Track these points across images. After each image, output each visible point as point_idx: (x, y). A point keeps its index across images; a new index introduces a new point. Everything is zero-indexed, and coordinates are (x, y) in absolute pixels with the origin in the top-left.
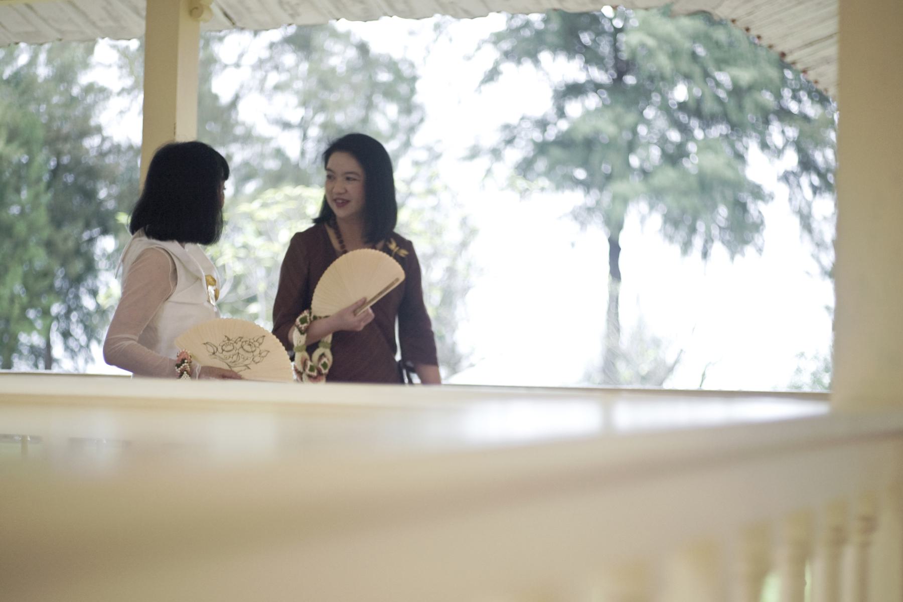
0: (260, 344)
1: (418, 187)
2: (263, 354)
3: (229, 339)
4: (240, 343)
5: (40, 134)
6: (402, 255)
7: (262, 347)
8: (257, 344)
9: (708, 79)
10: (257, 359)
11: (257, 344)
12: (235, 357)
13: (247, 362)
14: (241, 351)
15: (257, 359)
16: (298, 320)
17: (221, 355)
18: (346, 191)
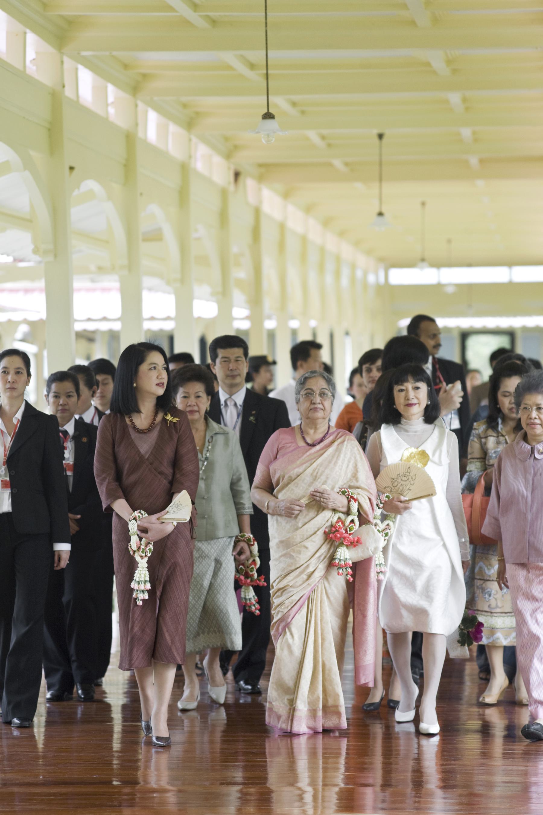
0: (410, 473)
1: (138, 576)
2: (414, 478)
3: (393, 479)
4: (399, 478)
5: (484, 641)
6: (138, 603)
7: (412, 474)
8: (408, 474)
9: (312, 732)
10: (412, 482)
11: (408, 474)
12: (401, 488)
13: (408, 487)
14: (402, 482)
15: (412, 482)
16: (251, 536)
17: (395, 490)
18: (68, 404)
